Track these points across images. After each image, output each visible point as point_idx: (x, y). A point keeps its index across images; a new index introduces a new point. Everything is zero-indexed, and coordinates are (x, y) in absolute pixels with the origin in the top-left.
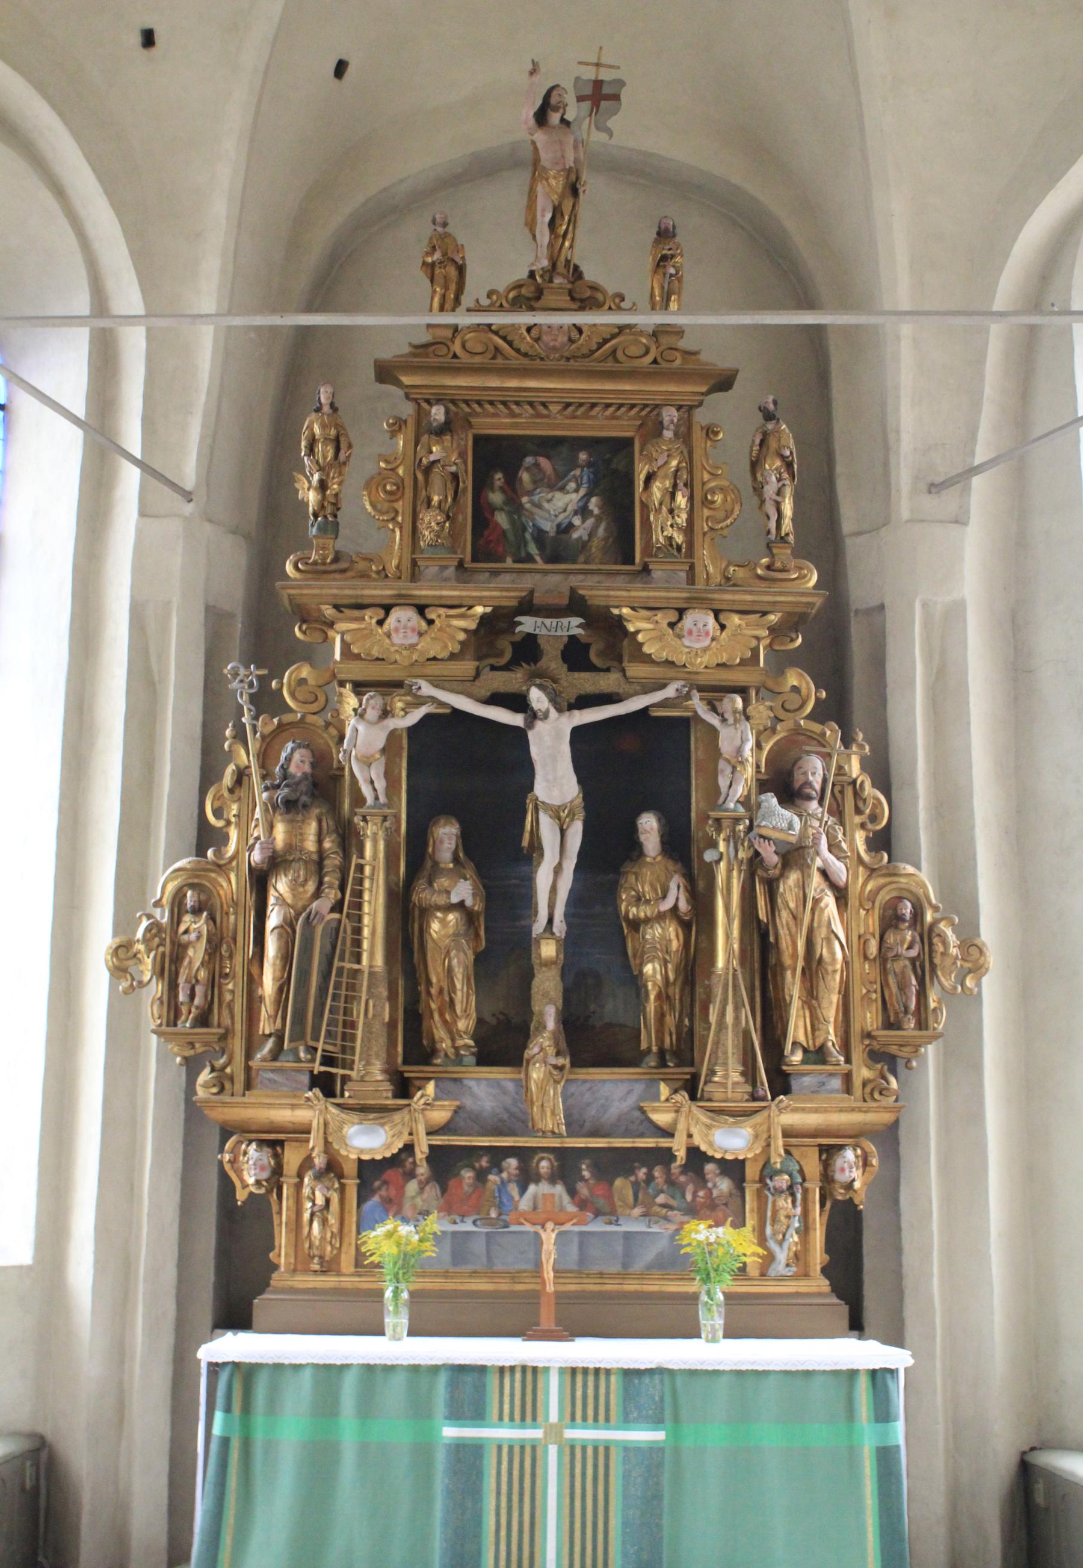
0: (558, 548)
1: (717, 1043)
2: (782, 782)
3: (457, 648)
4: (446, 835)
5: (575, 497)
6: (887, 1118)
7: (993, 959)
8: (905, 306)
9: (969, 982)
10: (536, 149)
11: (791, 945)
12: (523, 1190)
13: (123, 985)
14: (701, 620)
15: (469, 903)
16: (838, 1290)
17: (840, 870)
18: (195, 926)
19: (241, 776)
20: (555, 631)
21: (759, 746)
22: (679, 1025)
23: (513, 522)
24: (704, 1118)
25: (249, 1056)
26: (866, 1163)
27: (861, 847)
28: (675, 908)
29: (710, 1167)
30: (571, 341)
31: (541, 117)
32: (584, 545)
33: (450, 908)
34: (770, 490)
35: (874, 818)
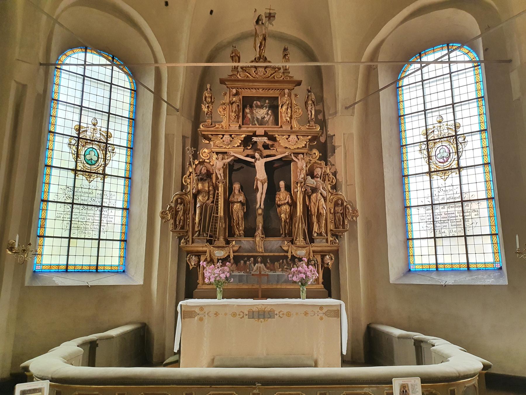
0: (261, 122)
1: (297, 232)
2: (311, 173)
3: (239, 144)
4: (237, 186)
5: (266, 111)
6: (336, 248)
7: (359, 213)
8: (340, 61)
9: (354, 218)
10: (256, 30)
11: (314, 209)
12: (254, 265)
13: (164, 220)
14: (293, 137)
15: (242, 201)
16: (325, 287)
17: (324, 193)
18: (180, 207)
19: (191, 173)
20: (261, 140)
21: (306, 166)
22: (289, 229)
23: (251, 116)
24: (295, 248)
25: (193, 236)
26: (331, 259)
27: (330, 189)
28: (288, 202)
29: (296, 260)
30: (264, 74)
31: (257, 22)
32: (268, 122)
33: (238, 202)
34: (309, 108)
35: (332, 182)
